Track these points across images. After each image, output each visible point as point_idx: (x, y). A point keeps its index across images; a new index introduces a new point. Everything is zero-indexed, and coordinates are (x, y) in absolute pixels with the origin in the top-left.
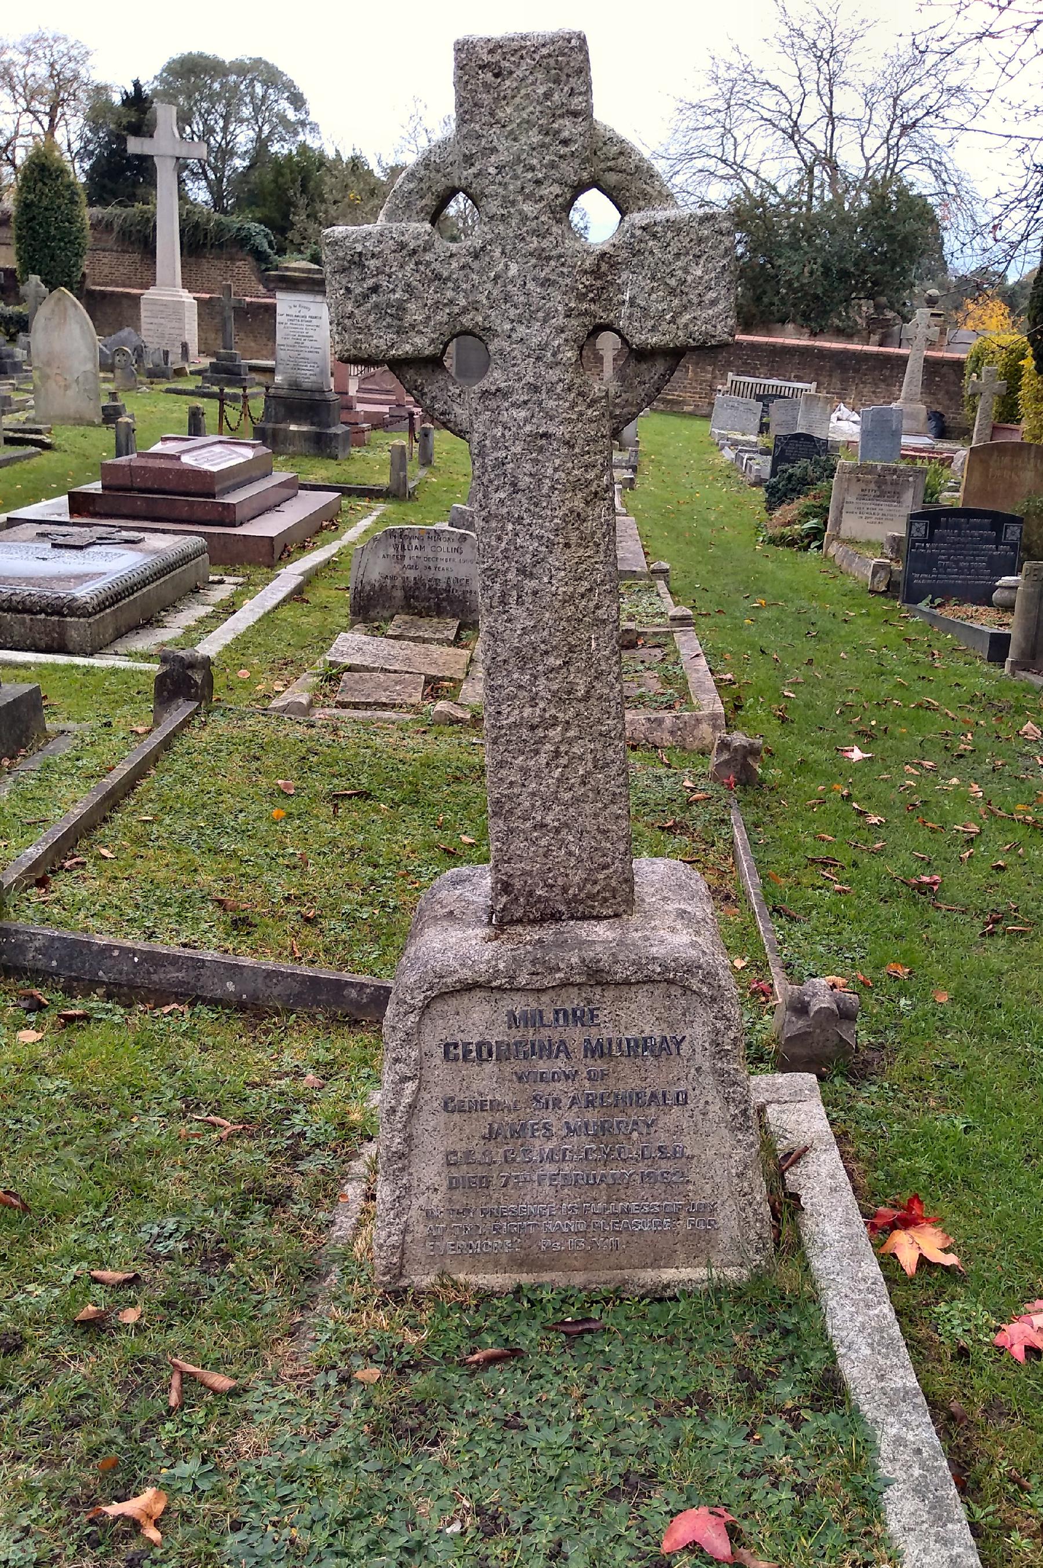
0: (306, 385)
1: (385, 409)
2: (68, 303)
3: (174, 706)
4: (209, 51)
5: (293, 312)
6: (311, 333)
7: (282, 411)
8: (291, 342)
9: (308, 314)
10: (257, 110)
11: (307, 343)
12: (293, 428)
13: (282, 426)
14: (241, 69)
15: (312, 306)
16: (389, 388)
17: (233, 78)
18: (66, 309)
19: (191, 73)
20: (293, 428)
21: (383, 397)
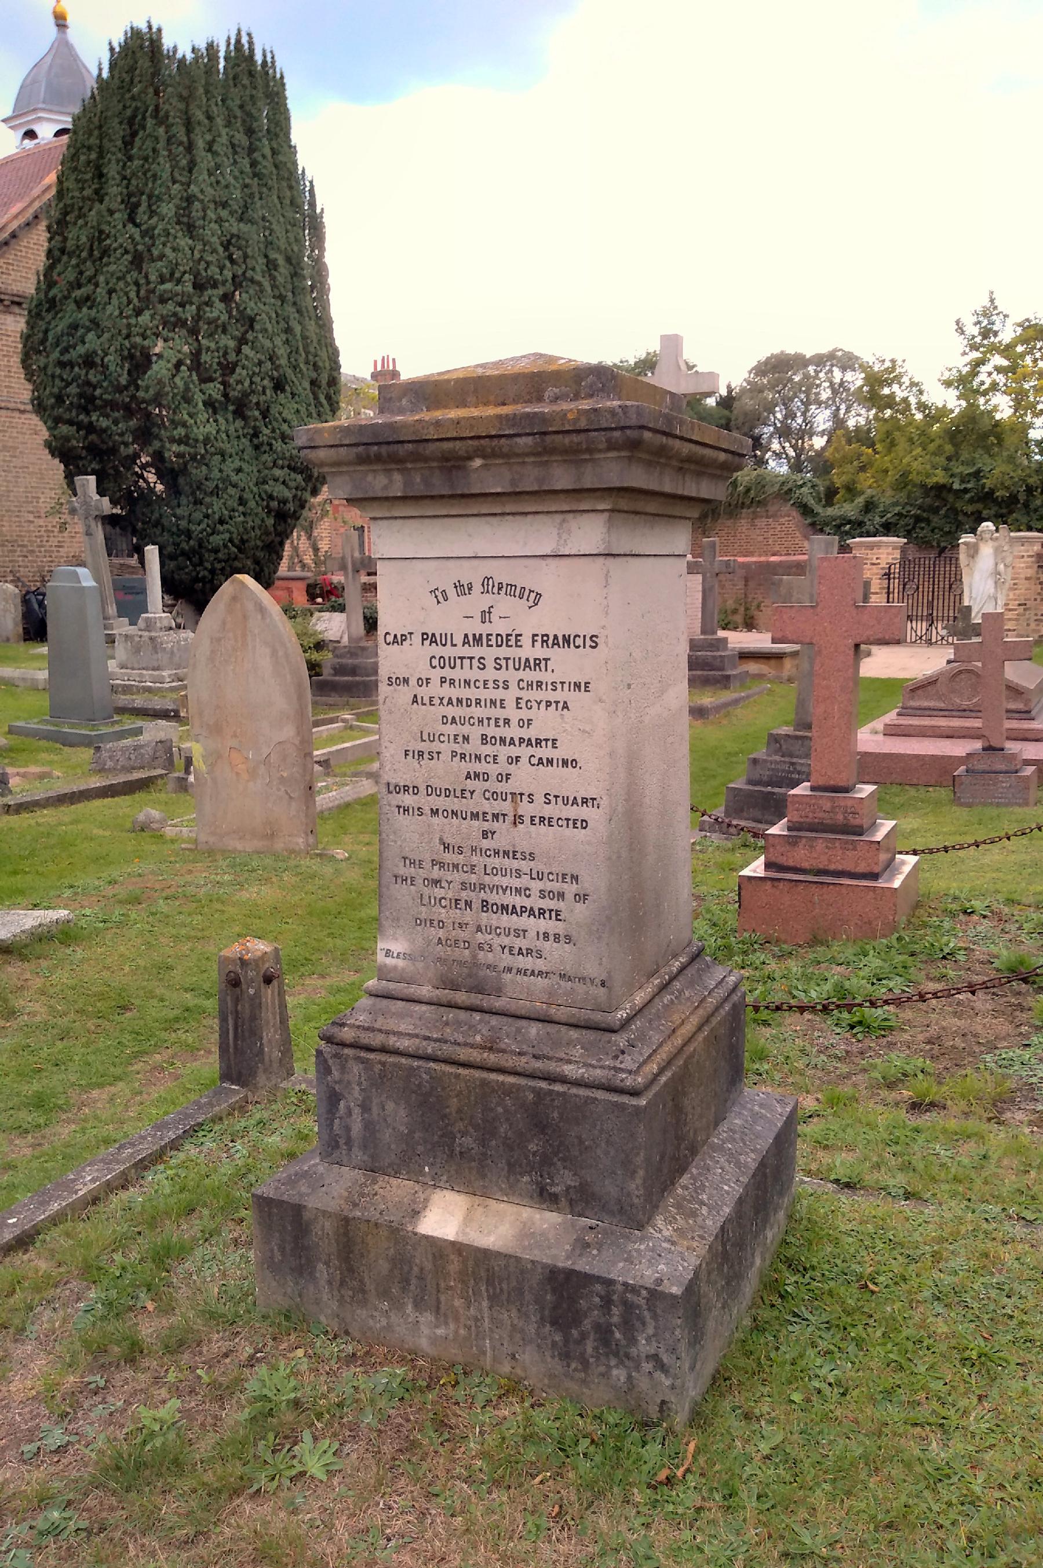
0: (523, 991)
1: (959, 749)
2: (250, 606)
3: (963, 557)
4: (791, 350)
5: (455, 618)
6: (545, 723)
7: (396, 1115)
8: (446, 771)
9: (530, 622)
10: (835, 392)
11: (524, 778)
12: (445, 1217)
13: (397, 1189)
14: (820, 360)
15: (545, 578)
16: (966, 703)
17: (811, 369)
18: (245, 617)
19: (778, 368)
20: (445, 1217)
21: (956, 723)
